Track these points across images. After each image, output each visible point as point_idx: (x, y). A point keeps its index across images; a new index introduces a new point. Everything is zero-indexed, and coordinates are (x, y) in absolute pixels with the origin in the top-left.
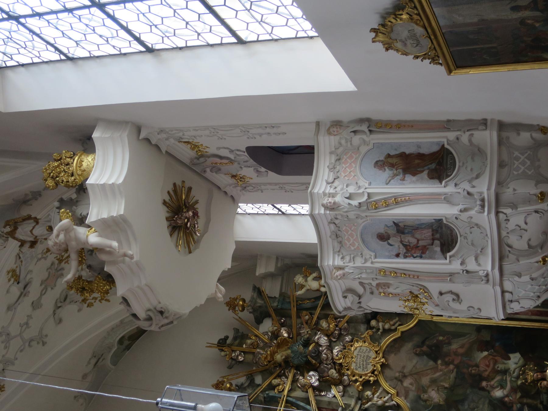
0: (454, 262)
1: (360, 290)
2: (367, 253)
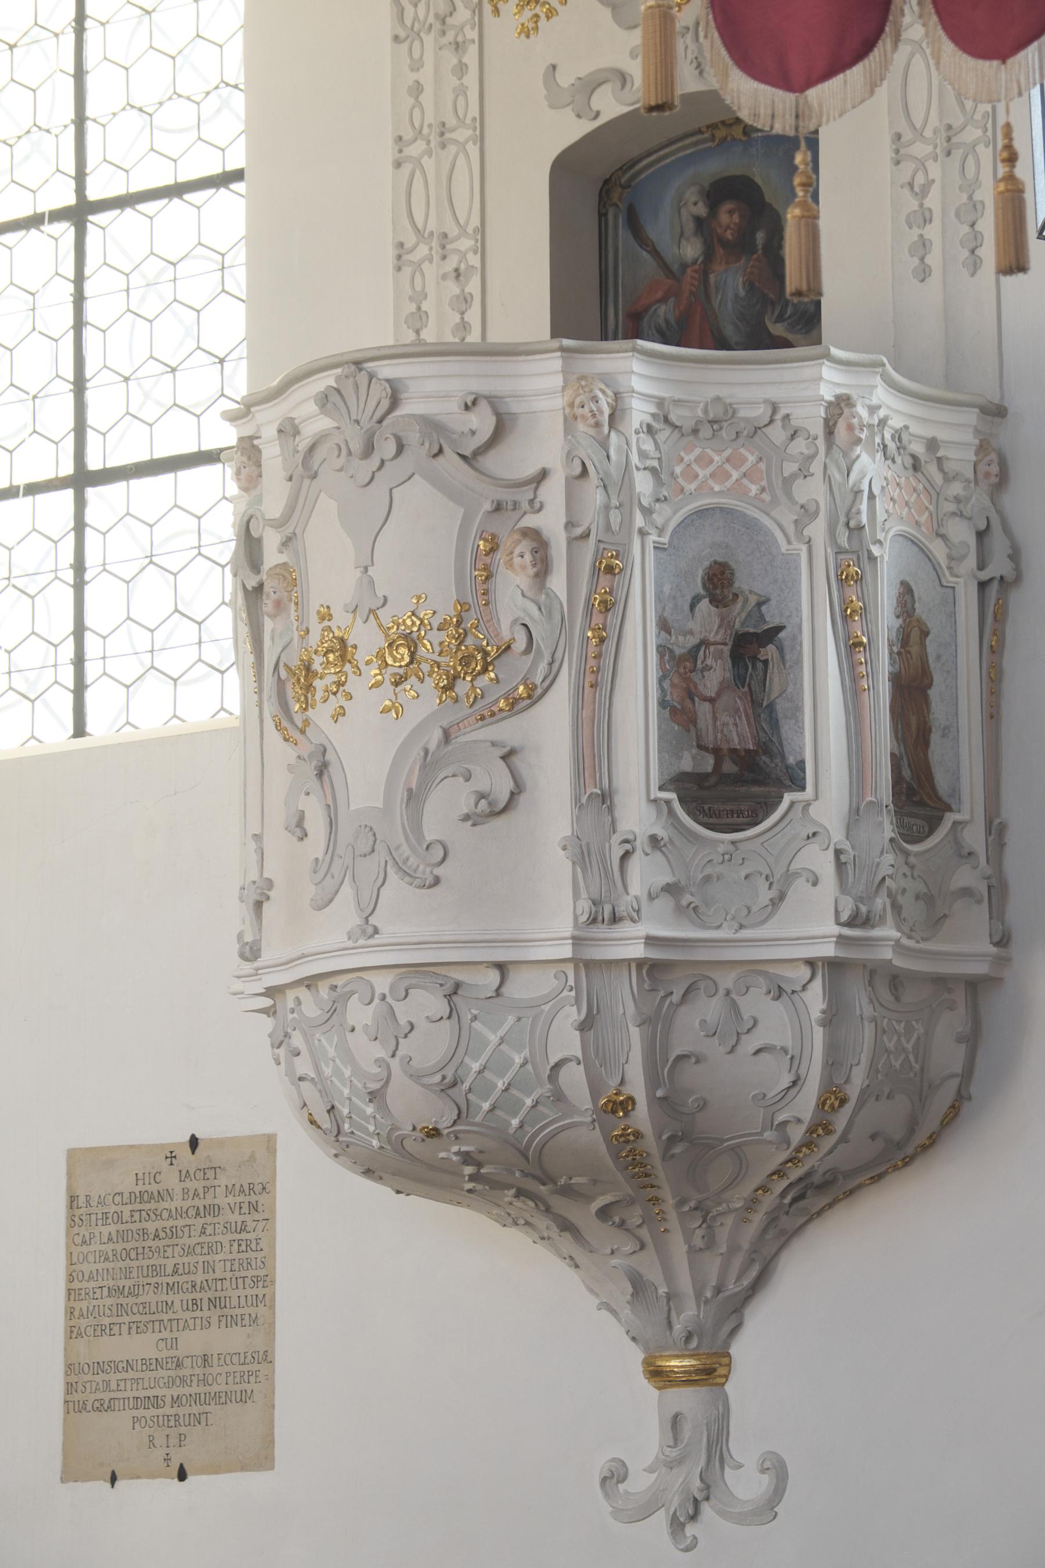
2: (670, 516)
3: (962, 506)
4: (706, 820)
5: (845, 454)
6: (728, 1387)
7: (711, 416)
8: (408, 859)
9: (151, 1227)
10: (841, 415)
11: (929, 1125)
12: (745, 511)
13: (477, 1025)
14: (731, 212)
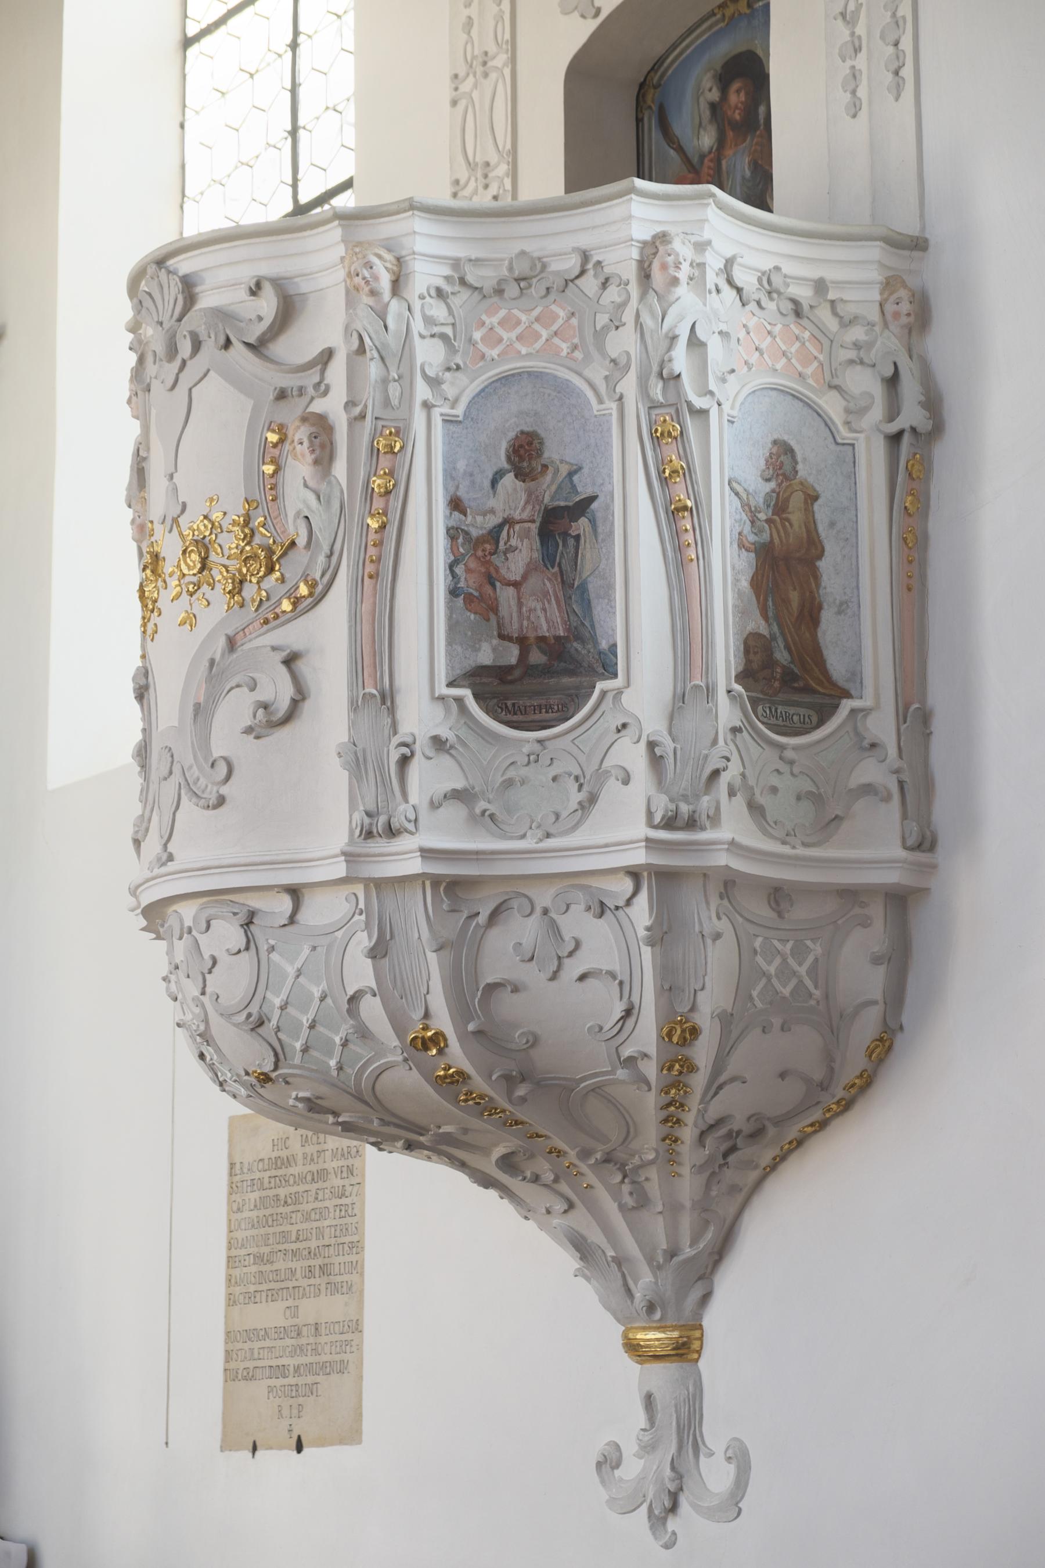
0: (439, 710)
1: (285, 348)
2: (464, 388)
3: (862, 353)
4: (510, 717)
5: (660, 298)
6: (702, 1364)
7: (516, 274)
8: (198, 779)
9: (282, 1192)
10: (655, 254)
11: (855, 1063)
12: (556, 373)
13: (274, 956)
14: (738, 91)
